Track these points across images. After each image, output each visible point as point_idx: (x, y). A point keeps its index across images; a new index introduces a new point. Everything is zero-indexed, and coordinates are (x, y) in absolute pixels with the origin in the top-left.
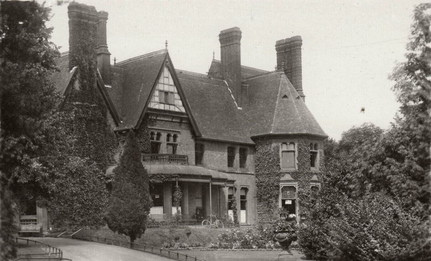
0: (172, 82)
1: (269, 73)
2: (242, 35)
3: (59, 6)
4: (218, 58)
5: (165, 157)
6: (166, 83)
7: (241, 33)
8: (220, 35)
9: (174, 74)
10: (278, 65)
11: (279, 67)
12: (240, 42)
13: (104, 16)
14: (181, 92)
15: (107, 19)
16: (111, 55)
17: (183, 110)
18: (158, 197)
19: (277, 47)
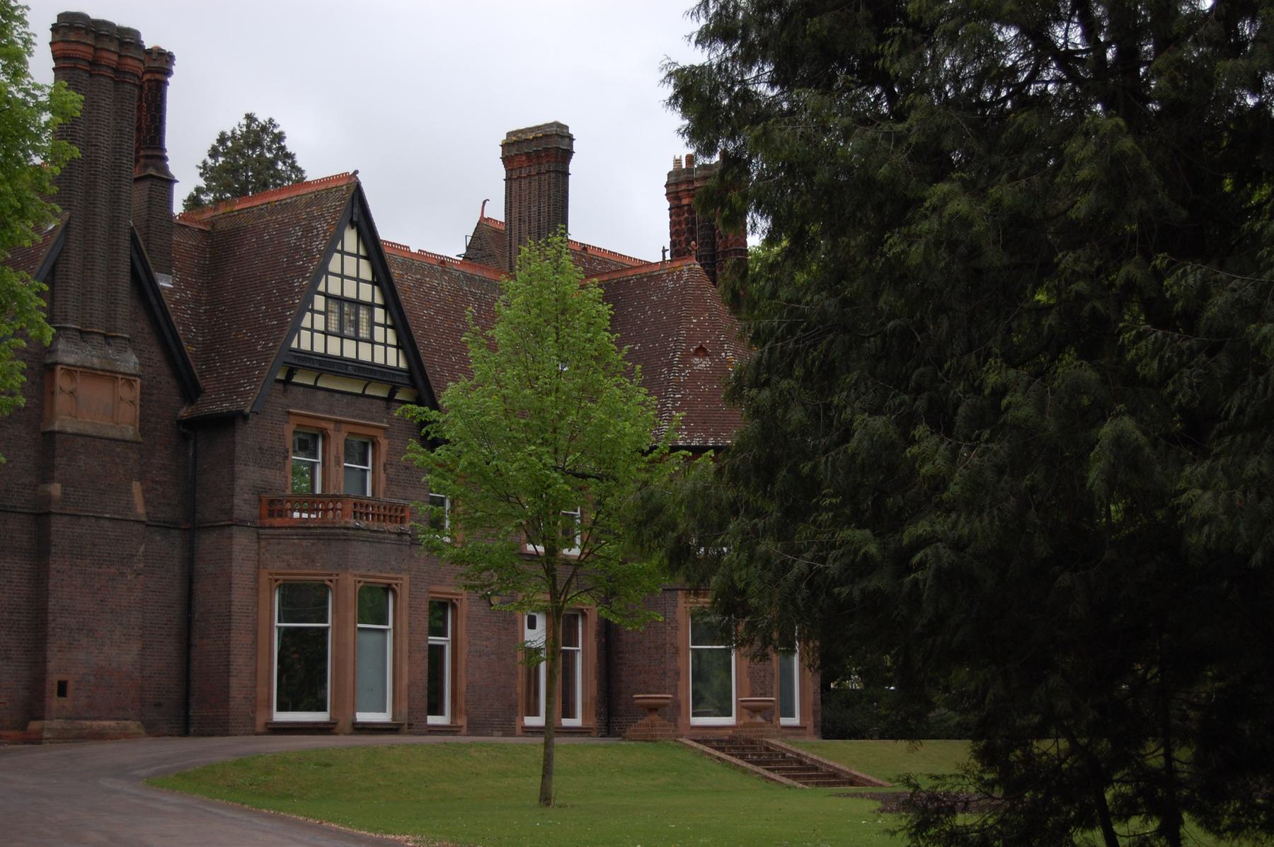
0: (366, 272)
1: (649, 264)
2: (576, 146)
3: (533, 115)
4: (497, 212)
5: (339, 505)
6: (348, 273)
7: (571, 138)
8: (505, 146)
9: (373, 248)
10: (673, 244)
11: (678, 248)
12: (165, 169)
13: (161, 63)
14: (392, 303)
15: (168, 73)
16: (176, 186)
17: (393, 358)
18: (764, 224)
19: (673, 189)
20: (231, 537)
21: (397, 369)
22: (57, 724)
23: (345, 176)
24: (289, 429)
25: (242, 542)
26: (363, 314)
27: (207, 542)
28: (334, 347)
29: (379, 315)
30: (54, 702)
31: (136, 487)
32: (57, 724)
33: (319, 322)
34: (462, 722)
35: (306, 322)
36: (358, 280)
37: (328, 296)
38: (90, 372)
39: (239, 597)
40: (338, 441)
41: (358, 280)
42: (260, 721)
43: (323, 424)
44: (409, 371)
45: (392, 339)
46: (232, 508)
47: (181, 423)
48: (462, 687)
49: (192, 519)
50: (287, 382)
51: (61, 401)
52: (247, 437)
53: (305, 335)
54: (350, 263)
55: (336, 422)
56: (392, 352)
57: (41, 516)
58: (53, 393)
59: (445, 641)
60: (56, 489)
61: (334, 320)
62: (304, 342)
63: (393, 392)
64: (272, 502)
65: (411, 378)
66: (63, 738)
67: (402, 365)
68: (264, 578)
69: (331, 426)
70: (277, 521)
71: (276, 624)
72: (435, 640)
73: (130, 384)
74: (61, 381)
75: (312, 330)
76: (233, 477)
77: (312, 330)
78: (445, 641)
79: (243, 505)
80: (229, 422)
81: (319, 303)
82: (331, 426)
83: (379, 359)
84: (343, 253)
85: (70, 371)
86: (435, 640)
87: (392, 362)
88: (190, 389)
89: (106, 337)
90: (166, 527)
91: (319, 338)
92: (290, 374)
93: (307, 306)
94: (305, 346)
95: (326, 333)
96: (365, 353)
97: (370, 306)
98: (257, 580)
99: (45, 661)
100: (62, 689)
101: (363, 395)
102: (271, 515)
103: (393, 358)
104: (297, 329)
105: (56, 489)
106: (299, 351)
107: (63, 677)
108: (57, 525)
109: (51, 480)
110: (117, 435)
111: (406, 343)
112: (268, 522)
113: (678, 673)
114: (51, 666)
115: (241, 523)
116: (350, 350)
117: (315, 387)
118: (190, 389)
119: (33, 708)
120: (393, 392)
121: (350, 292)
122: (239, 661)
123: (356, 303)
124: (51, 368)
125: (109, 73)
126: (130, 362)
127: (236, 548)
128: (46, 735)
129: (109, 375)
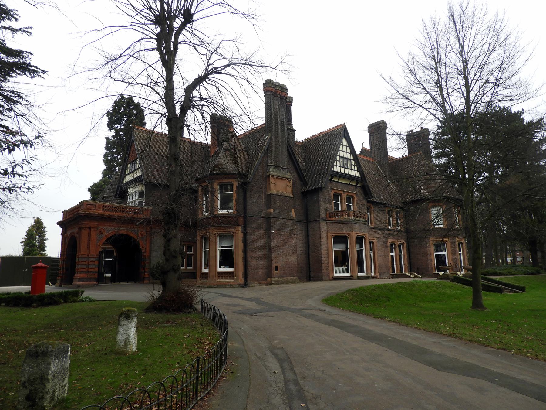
15: (292, 103)
17: (357, 174)
20: (320, 223)
21: (358, 177)
22: (276, 279)
23: (342, 125)
24: (332, 193)
25: (323, 224)
26: (349, 162)
27: (312, 225)
28: (342, 170)
29: (353, 162)
30: (275, 272)
31: (293, 210)
32: (276, 279)
33: (338, 164)
34: (378, 274)
35: (335, 164)
36: (347, 153)
37: (340, 157)
38: (279, 178)
39: (323, 240)
40: (344, 196)
41: (347, 153)
42: (331, 276)
43: (341, 192)
44: (361, 177)
45: (356, 169)
46: (319, 215)
47: (302, 193)
48: (377, 265)
49: (308, 219)
50: (331, 180)
51: (272, 186)
52: (322, 196)
53: (335, 167)
54: (345, 147)
55: (344, 191)
56: (356, 172)
57: (268, 219)
58: (269, 183)
59: (393, 254)
60: (272, 210)
61: (342, 163)
62: (335, 169)
63: (357, 184)
64: (330, 213)
65: (362, 180)
66: (278, 283)
67: (359, 176)
68: (329, 235)
69: (342, 193)
70: (332, 219)
71: (446, 253)
72: (391, 254)
73: (289, 181)
74: (272, 180)
75: (337, 166)
76: (319, 207)
77: (337, 166)
78: (393, 254)
79: (322, 214)
80: (319, 190)
81: (338, 158)
82: (342, 193)
83: (354, 174)
84: (343, 145)
85: (273, 176)
86: (391, 254)
87: (357, 175)
88: (305, 184)
89: (282, 168)
90: (300, 222)
91: (339, 168)
92: (332, 178)
93: (335, 159)
94: (335, 170)
95: (340, 167)
96: (350, 173)
97: (351, 160)
98: (327, 236)
99: (271, 260)
100: (276, 268)
101: (349, 184)
102: (330, 217)
103: (357, 174)
104: (333, 165)
105: (272, 210)
106: (334, 171)
107: (276, 265)
108: (273, 220)
109: (270, 208)
110: (287, 195)
111: (360, 170)
112: (329, 219)
113: (432, 260)
114: (273, 262)
115: (322, 220)
116: (346, 171)
117: (338, 182)
118: (305, 184)
119: (269, 274)
120: (357, 184)
121: (345, 156)
122: (324, 259)
123: (347, 159)
124: (268, 177)
125: (279, 96)
126: (288, 175)
127: (321, 227)
128: (273, 282)
129: (283, 178)
